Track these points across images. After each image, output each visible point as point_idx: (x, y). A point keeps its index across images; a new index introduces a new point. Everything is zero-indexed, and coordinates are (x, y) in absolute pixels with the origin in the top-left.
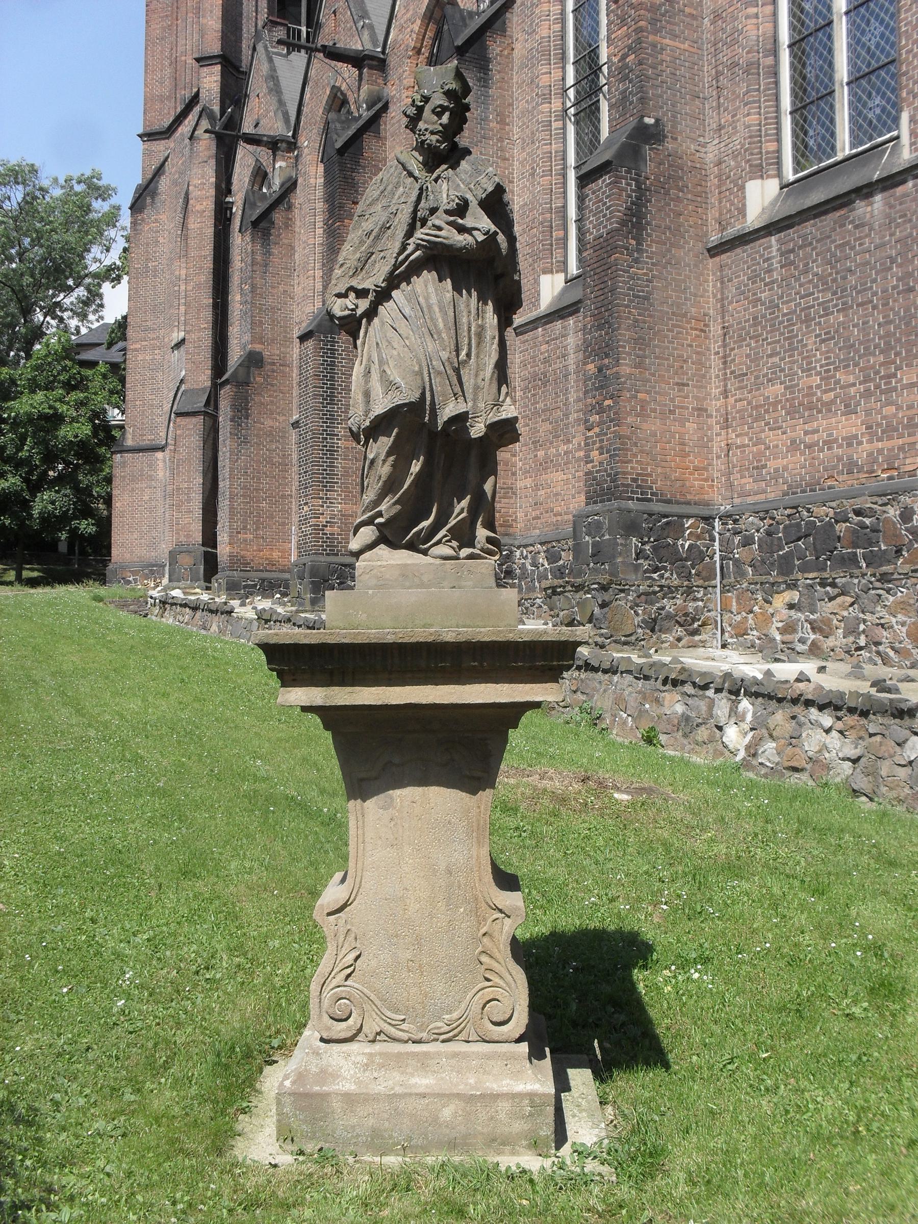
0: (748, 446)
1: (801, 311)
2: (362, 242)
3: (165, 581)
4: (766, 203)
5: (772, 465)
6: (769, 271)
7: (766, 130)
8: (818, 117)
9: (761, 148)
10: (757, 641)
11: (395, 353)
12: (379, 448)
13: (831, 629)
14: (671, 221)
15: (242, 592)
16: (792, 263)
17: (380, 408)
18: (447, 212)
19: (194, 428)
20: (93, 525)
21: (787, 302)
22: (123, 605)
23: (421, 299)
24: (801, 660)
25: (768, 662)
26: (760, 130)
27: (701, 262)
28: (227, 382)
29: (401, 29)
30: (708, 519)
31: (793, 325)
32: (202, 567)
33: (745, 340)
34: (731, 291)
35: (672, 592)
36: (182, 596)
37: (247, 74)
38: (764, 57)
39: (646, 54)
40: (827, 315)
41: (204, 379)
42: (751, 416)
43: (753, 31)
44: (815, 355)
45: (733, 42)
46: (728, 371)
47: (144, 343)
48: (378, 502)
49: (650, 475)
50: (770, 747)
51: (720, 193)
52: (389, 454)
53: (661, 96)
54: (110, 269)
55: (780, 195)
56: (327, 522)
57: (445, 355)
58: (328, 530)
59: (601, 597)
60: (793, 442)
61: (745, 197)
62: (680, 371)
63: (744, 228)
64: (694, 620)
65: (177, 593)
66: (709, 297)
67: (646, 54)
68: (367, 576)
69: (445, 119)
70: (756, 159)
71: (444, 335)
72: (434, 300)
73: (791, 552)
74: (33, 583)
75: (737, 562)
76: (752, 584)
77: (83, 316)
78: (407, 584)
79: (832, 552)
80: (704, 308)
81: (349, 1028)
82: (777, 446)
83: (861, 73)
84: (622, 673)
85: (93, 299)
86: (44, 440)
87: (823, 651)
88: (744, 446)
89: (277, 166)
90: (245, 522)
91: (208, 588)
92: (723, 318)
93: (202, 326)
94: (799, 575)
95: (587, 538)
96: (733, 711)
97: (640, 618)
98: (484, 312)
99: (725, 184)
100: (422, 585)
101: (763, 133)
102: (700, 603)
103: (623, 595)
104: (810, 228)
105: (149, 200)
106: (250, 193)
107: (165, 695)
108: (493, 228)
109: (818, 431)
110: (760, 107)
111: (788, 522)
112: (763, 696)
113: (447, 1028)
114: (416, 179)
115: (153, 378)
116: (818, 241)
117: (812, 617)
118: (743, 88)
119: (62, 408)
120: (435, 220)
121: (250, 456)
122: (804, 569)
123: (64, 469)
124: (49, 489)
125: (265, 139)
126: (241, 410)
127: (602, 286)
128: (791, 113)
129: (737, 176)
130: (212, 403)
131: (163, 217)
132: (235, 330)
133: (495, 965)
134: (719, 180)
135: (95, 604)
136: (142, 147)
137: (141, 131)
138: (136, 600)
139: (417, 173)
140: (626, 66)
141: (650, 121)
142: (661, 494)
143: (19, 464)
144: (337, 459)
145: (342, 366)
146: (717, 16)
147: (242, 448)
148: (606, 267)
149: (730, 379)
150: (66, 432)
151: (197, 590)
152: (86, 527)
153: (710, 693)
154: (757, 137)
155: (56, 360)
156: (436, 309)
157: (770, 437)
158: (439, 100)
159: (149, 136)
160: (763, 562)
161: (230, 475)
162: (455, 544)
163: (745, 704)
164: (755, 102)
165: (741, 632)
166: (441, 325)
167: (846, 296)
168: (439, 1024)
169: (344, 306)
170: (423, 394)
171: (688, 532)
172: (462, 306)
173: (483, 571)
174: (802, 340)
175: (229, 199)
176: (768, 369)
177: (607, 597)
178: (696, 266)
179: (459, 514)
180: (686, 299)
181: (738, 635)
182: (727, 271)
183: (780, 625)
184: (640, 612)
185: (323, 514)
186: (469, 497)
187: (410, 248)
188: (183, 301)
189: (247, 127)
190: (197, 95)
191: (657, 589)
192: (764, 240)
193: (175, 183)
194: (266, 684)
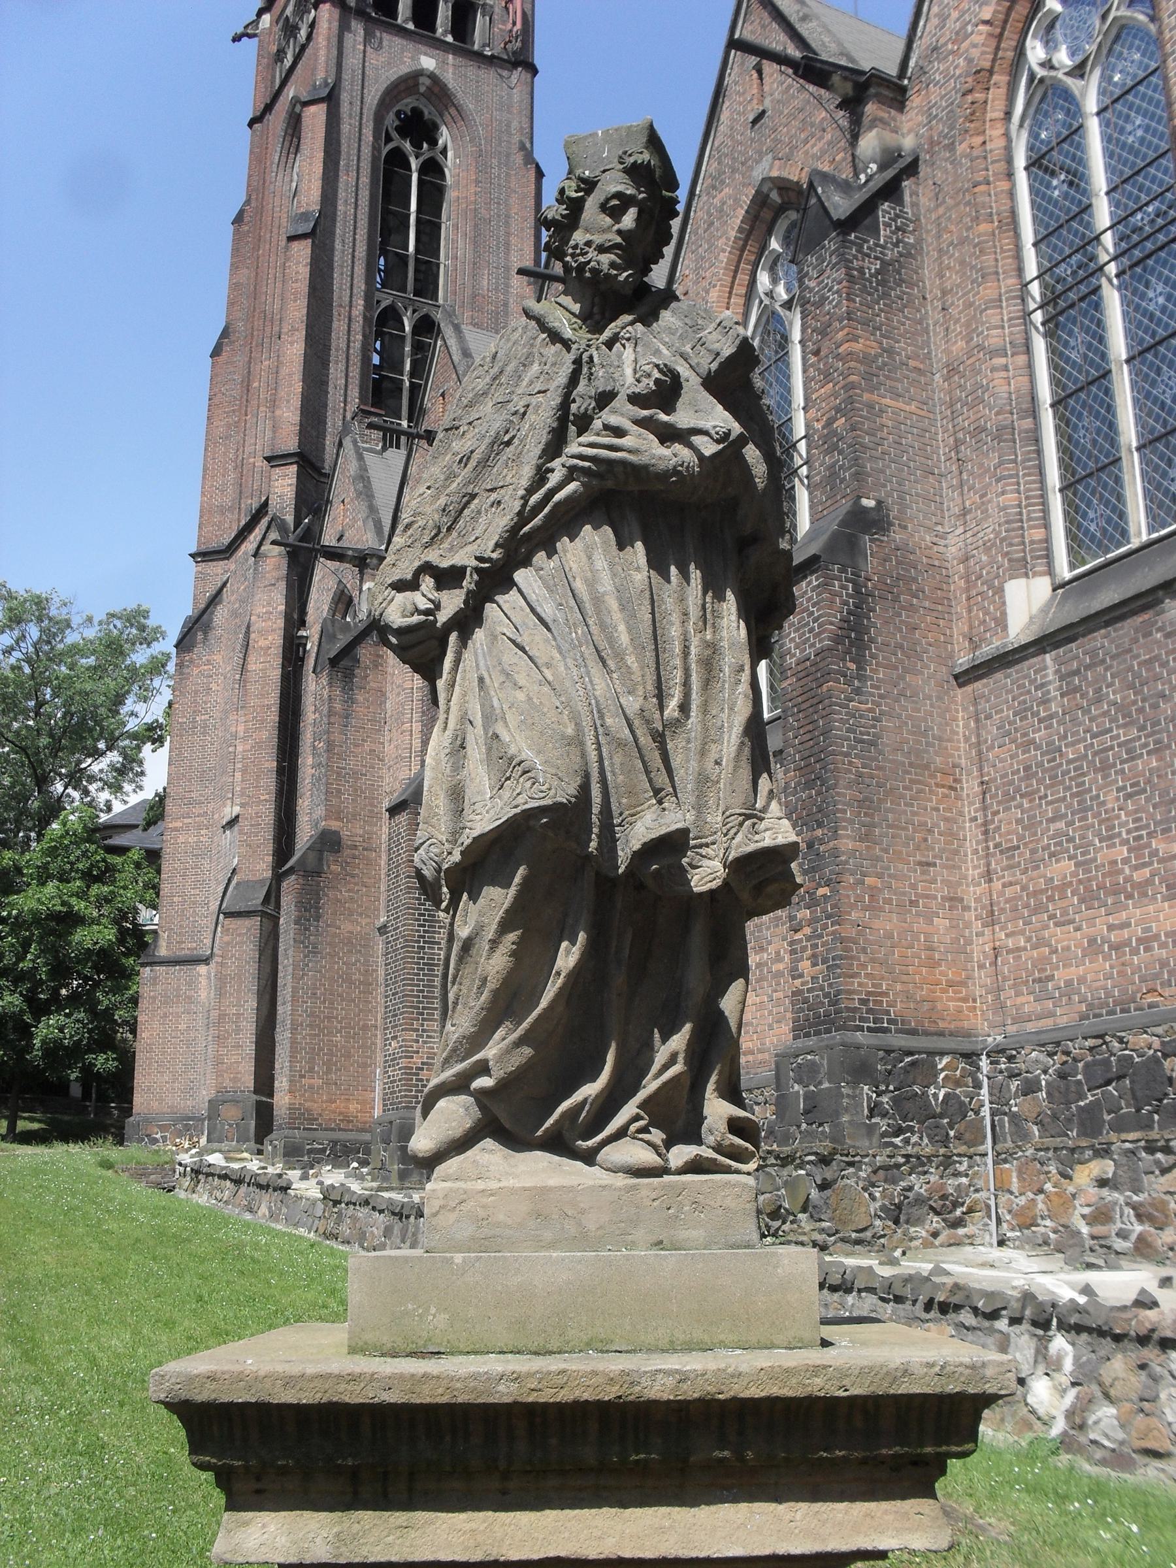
0: (1025, 949)
1: (1095, 754)
2: (450, 477)
3: (203, 1141)
4: (1034, 611)
5: (1061, 975)
6: (1045, 702)
7: (1029, 512)
8: (1100, 493)
9: (1023, 536)
10: (1052, 1236)
11: (521, 696)
12: (481, 914)
13: (1167, 1216)
14: (903, 638)
15: (306, 1158)
16: (1077, 689)
17: (484, 819)
18: (634, 399)
19: (250, 928)
20: (113, 1060)
21: (1073, 744)
22: (140, 1174)
23: (579, 585)
24: (1123, 1263)
25: (1076, 1269)
26: (1020, 514)
27: (947, 693)
28: (291, 870)
30: (970, 1057)
31: (1083, 775)
32: (253, 1123)
33: (1014, 798)
34: (991, 730)
35: (924, 1165)
36: (223, 1163)
37: (330, 477)
38: (1018, 419)
39: (861, 416)
40: (1133, 759)
41: (262, 867)
42: (1027, 906)
43: (1002, 386)
44: (1118, 817)
45: (976, 402)
46: (991, 844)
47: (186, 821)
48: (478, 1039)
49: (886, 994)
50: (1105, 1414)
51: (968, 599)
52: (505, 926)
53: (883, 472)
54: (150, 728)
55: (1053, 598)
56: (423, 1063)
57: (632, 704)
59: (820, 1174)
60: (1092, 941)
61: (1004, 603)
62: (923, 846)
63: (1005, 645)
64: (956, 1204)
65: (216, 1159)
66: (959, 742)
67: (861, 416)
68: (452, 1217)
69: (629, 220)
70: (1017, 552)
71: (631, 660)
72: (606, 585)
73: (1096, 1104)
74: (27, 1138)
75: (1014, 1117)
76: (1040, 1150)
77: (116, 788)
78: (548, 1235)
79: (1160, 1100)
80: (952, 756)
82: (1068, 948)
83: (1156, 435)
84: (860, 1291)
85: (129, 768)
86: (53, 946)
87: (1156, 1251)
88: (1018, 949)
89: (365, 587)
90: (311, 1061)
91: (260, 1152)
92: (981, 769)
93: (262, 798)
94: (1113, 1137)
95: (796, 1087)
96: (1042, 1353)
97: (878, 1204)
98: (717, 615)
99: (975, 585)
100: (583, 1240)
101: (1025, 517)
102: (964, 1180)
103: (852, 1170)
104: (1100, 639)
105: (200, 636)
106: (329, 622)
107: (170, 1324)
108: (737, 428)
109: (1128, 925)
110: (1018, 484)
111: (1090, 1058)
112: (1089, 1330)
114: (567, 344)
116: (1112, 658)
117: (1135, 1198)
118: (994, 459)
119: (79, 905)
120: (609, 417)
121: (320, 972)
122: (1119, 1126)
123: (79, 986)
124: (58, 1011)
125: (350, 553)
126: (310, 909)
127: (810, 727)
128: (1061, 490)
129: (992, 576)
130: (273, 899)
131: (217, 658)
132: (306, 803)
134: (967, 582)
135: (101, 1172)
136: (195, 569)
137: (194, 550)
138: (160, 1168)
139: (568, 333)
140: (834, 433)
141: (868, 503)
142: (903, 1021)
143: (18, 978)
146: (952, 370)
147: (310, 961)
148: (815, 701)
149: (994, 855)
150: (83, 937)
151: (245, 1155)
152: (103, 1062)
153: (1002, 1324)
154: (1017, 522)
155: (75, 843)
156: (613, 604)
157: (1055, 934)
158: (615, 183)
159: (203, 556)
160: (1055, 1117)
161: (293, 997)
162: (657, 1136)
163: (1060, 1343)
164: (1011, 476)
165: (1027, 1222)
166: (624, 639)
167: (1159, 732)
169: (410, 608)
170: (585, 788)
171: (942, 1075)
172: (669, 602)
173: (728, 1202)
174: (1098, 796)
175: (302, 633)
176: (1050, 838)
177: (829, 1173)
178: (939, 698)
179: (665, 1067)
180: (928, 744)
181: (1021, 1227)
182: (983, 705)
183: (1086, 1211)
184: (877, 1195)
186: (688, 1027)
187: (554, 479)
188: (239, 766)
189: (329, 539)
190: (265, 504)
191: (901, 1160)
192: (1035, 660)
193: (235, 614)
194: (325, 1306)
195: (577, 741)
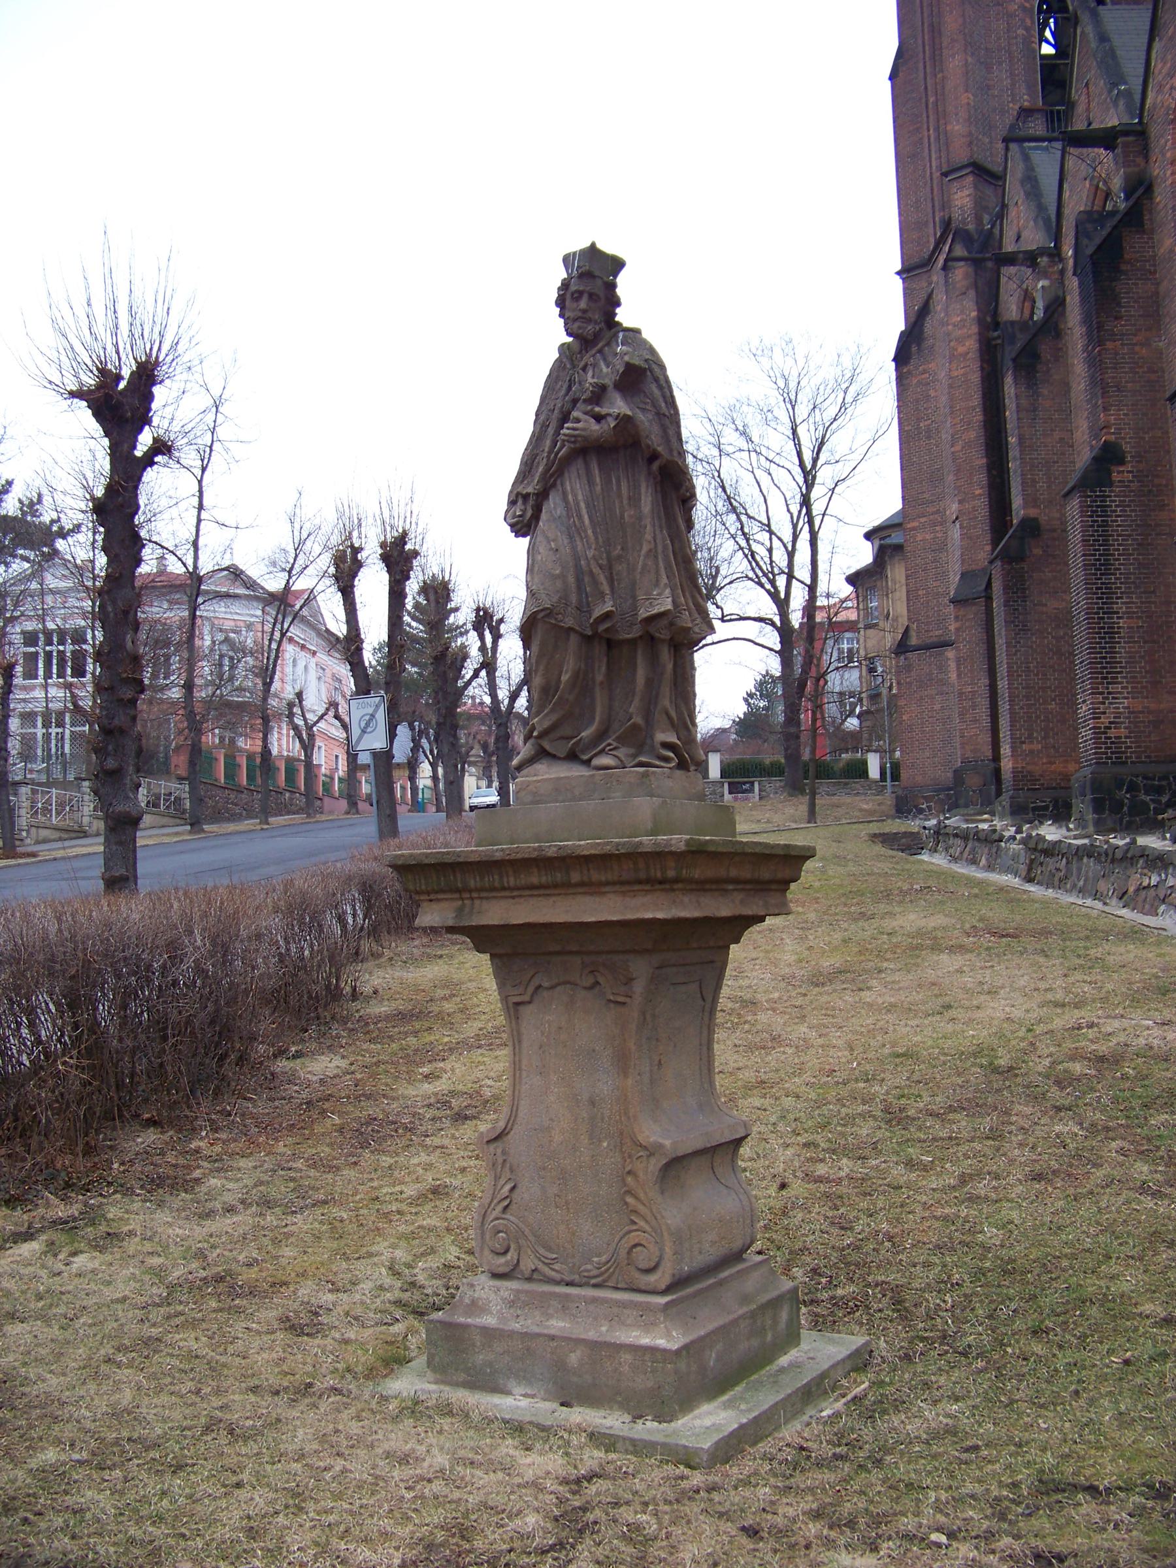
19: (974, 613)
29: (1160, 90)
56: (1110, 723)
58: (1112, 733)
78: (560, 798)
81: (507, 1262)
105: (914, 349)
113: (595, 1272)
115: (935, 561)
133: (640, 1208)
144: (1119, 643)
145: (1119, 526)
168: (589, 1267)
173: (632, 780)
185: (1104, 713)
195: (562, 576)
